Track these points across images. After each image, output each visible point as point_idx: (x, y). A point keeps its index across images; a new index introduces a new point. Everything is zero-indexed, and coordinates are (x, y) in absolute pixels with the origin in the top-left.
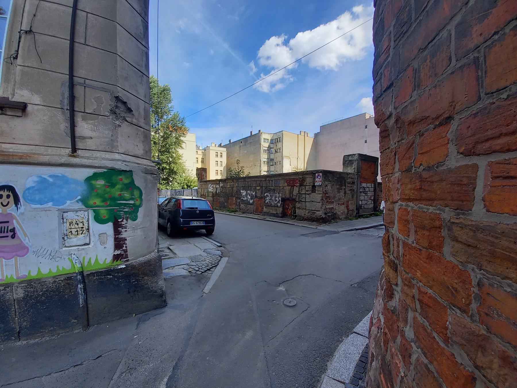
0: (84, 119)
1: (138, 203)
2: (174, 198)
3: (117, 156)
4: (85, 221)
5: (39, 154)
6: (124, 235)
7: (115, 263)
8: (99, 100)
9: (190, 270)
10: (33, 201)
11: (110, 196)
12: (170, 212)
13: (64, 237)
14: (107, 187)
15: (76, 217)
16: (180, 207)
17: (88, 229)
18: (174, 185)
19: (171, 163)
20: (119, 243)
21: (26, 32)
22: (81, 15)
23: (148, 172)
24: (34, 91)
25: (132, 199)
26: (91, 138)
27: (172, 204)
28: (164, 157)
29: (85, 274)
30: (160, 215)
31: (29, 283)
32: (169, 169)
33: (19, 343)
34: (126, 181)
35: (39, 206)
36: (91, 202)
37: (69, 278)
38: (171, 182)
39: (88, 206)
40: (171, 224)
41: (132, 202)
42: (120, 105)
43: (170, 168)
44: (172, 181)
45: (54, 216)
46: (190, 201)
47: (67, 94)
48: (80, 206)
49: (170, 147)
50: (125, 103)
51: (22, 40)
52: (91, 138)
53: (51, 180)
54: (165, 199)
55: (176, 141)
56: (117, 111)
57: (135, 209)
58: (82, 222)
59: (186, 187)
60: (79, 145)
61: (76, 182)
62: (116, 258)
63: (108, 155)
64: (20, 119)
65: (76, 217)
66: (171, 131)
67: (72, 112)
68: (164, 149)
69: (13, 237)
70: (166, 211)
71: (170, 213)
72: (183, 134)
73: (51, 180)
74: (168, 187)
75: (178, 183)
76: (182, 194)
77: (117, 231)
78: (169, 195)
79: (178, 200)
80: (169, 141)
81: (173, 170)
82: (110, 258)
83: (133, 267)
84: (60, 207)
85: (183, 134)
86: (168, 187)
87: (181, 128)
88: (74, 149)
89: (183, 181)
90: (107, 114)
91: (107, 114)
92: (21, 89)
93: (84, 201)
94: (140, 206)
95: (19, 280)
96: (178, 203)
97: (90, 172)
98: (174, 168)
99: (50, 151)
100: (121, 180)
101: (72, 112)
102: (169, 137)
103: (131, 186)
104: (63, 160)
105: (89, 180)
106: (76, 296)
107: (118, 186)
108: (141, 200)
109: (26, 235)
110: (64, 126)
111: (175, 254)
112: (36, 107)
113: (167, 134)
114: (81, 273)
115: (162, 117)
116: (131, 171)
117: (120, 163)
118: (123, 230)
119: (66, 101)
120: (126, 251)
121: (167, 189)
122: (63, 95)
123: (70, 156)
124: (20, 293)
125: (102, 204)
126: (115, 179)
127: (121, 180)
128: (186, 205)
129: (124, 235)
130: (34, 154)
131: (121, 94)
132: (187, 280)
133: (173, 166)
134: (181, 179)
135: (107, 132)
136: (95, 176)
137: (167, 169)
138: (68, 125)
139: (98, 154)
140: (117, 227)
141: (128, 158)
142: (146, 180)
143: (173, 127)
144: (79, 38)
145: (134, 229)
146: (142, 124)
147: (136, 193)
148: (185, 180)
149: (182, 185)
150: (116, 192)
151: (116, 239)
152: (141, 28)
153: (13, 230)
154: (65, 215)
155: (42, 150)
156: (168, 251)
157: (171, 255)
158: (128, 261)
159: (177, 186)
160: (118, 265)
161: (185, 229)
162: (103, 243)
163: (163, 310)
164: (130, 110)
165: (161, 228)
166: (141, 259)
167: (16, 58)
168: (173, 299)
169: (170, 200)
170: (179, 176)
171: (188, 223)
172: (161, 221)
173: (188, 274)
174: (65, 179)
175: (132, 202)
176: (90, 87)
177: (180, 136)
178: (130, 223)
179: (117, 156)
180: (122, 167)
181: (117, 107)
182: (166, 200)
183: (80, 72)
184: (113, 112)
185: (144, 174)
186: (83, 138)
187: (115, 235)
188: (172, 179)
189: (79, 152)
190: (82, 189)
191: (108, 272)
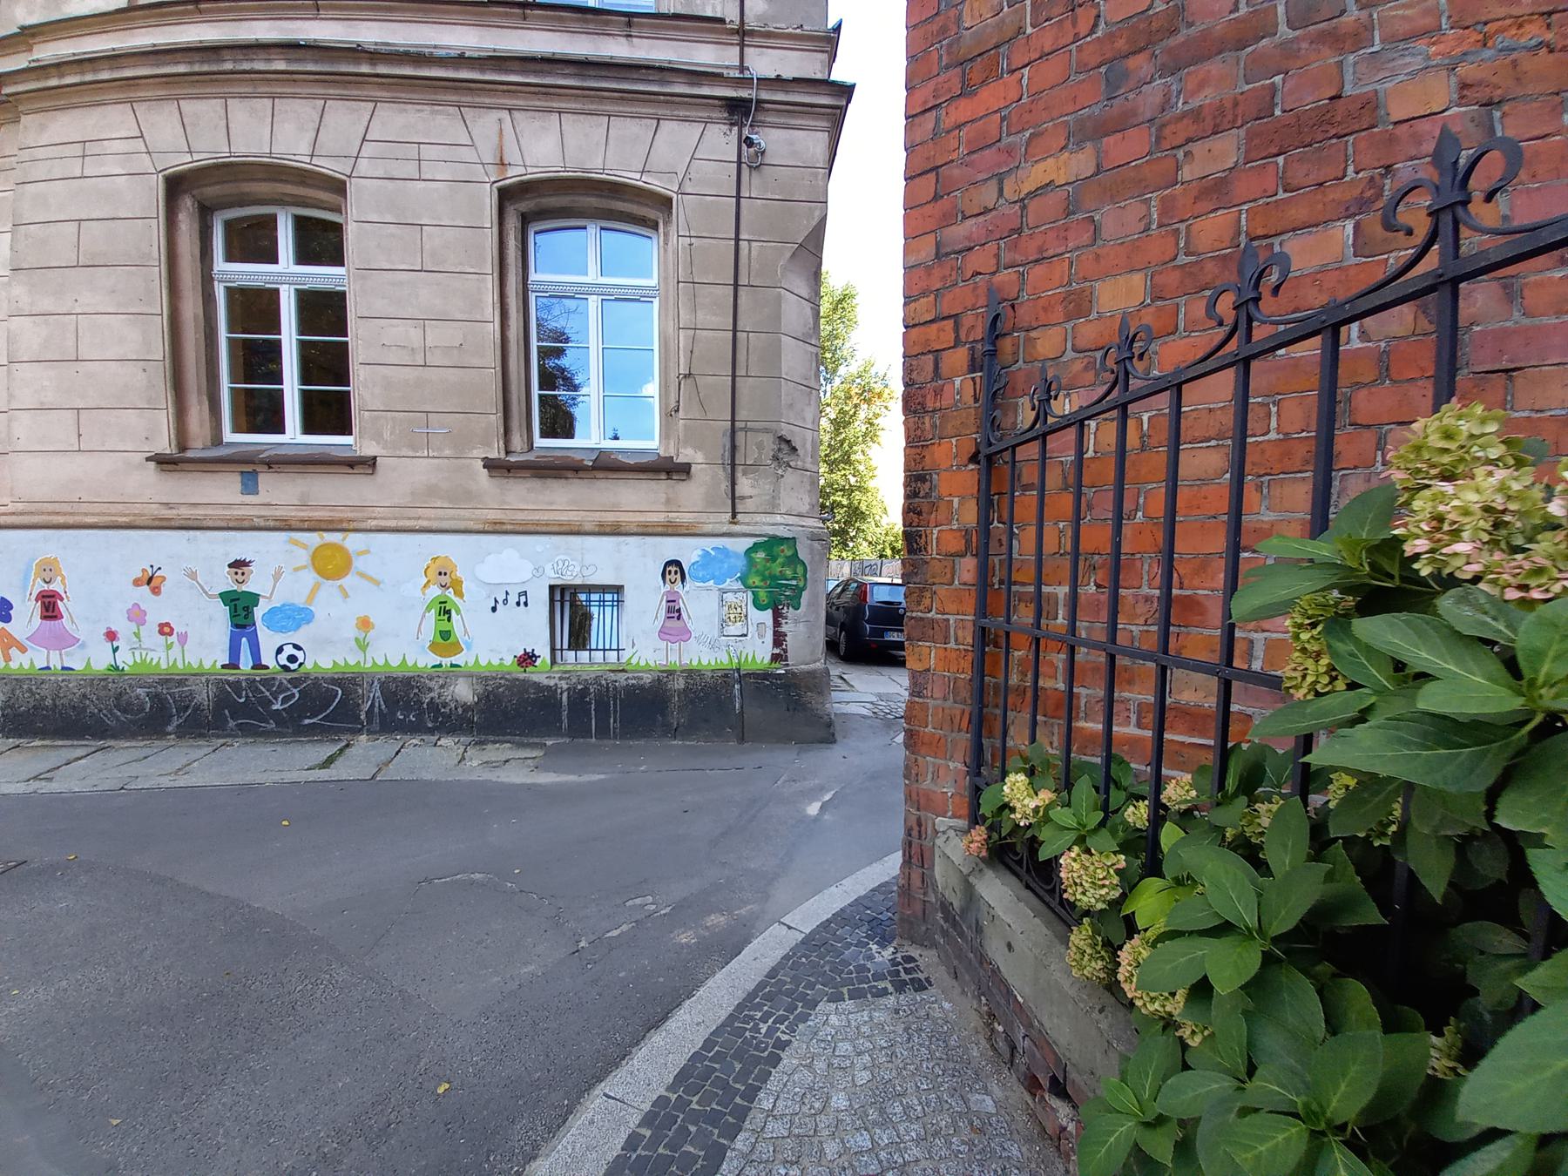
0: (745, 474)
1: (801, 584)
2: (857, 581)
3: (778, 519)
4: (744, 607)
5: (702, 523)
6: (784, 628)
7: (773, 665)
8: (760, 446)
9: (876, 710)
10: (697, 579)
11: (770, 574)
12: (846, 610)
13: (723, 623)
14: (768, 560)
15: (735, 600)
16: (865, 600)
17: (746, 616)
18: (861, 548)
19: (853, 491)
20: (779, 639)
21: (685, 376)
22: (741, 336)
23: (815, 537)
24: (697, 448)
25: (794, 578)
26: (751, 497)
27: (849, 594)
28: (836, 476)
29: (742, 673)
30: (830, 620)
31: (690, 673)
32: (849, 506)
33: (675, 742)
34: (789, 553)
35: (702, 584)
36: (750, 582)
37: (726, 676)
38: (852, 540)
39: (747, 587)
40: (846, 636)
41: (794, 583)
42: (784, 446)
43: (850, 504)
44: (855, 537)
45: (715, 595)
46: (889, 587)
47: (728, 446)
48: (739, 585)
49: (851, 448)
50: (788, 442)
51: (682, 386)
52: (751, 497)
53: (713, 553)
54: (837, 583)
55: (867, 429)
56: (781, 456)
57: (798, 591)
58: (741, 607)
59: (888, 552)
60: (739, 508)
61: (736, 555)
62: (775, 658)
63: (769, 519)
64: (685, 483)
65: (735, 600)
66: (856, 406)
67: (733, 465)
68: (836, 456)
69: (679, 618)
70: (838, 609)
71: (845, 612)
72: (886, 408)
73: (713, 553)
74: (844, 554)
75: (870, 543)
76: (878, 573)
77: (777, 624)
78: (846, 571)
79: (862, 586)
80: (849, 433)
81: (857, 508)
82: (768, 658)
83: (794, 674)
84: (720, 587)
85: (886, 408)
86: (844, 554)
87: (880, 395)
88: (734, 515)
89: (883, 538)
90: (769, 462)
91: (769, 462)
92: (685, 448)
93: (742, 579)
94: (804, 589)
95: (681, 669)
96: (862, 590)
97: (750, 542)
98: (859, 503)
99: (712, 518)
100: (783, 551)
101: (733, 465)
102: (850, 423)
103: (794, 560)
104: (725, 529)
105: (749, 551)
106: (732, 699)
107: (780, 560)
108: (806, 579)
109: (690, 618)
110: (725, 485)
111: (852, 686)
112: (699, 466)
113: (846, 413)
114: (738, 670)
115: (835, 371)
116: (794, 538)
117: (782, 527)
118: (784, 621)
119: (727, 454)
120: (785, 651)
121: (843, 559)
122: (725, 446)
123: (731, 523)
124: (680, 684)
125: (762, 584)
126: (777, 550)
127: (783, 551)
128: (880, 596)
129: (784, 628)
130: (698, 523)
131: (785, 431)
132: (868, 721)
133: (857, 498)
134: (878, 530)
135: (767, 487)
136: (755, 548)
137: (843, 506)
138: (729, 484)
139: (758, 518)
140: (777, 617)
141: (791, 520)
142: (812, 549)
143: (861, 395)
144: (741, 372)
145: (796, 622)
146: (808, 466)
147: (800, 569)
148: (887, 534)
149: (879, 547)
150: (776, 568)
151: (775, 633)
152: (811, 321)
153: (679, 610)
154: (725, 595)
155: (703, 518)
156: (841, 681)
157: (844, 686)
158: (787, 665)
159: (868, 550)
160: (777, 669)
161: (874, 646)
162: (761, 636)
163: (831, 746)
164: (794, 449)
165: (831, 646)
166: (803, 667)
167: (677, 411)
168: (844, 737)
169: (845, 585)
170: (873, 523)
171: (881, 633)
172: (833, 630)
173: (872, 715)
174: (723, 551)
175: (794, 583)
176: (751, 430)
177: (876, 416)
178: (790, 613)
179: (778, 519)
180: (782, 532)
181: (779, 450)
182: (838, 586)
183: (742, 414)
184: (775, 458)
185: (809, 542)
186: (743, 498)
187: (774, 627)
188: (854, 533)
189: (739, 517)
190: (741, 563)
191: (765, 676)
